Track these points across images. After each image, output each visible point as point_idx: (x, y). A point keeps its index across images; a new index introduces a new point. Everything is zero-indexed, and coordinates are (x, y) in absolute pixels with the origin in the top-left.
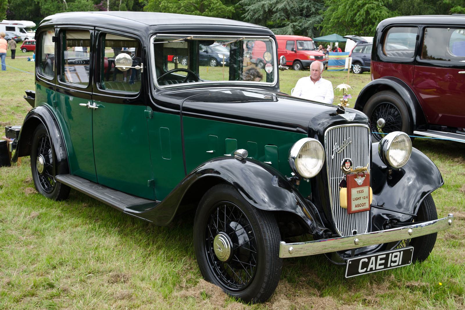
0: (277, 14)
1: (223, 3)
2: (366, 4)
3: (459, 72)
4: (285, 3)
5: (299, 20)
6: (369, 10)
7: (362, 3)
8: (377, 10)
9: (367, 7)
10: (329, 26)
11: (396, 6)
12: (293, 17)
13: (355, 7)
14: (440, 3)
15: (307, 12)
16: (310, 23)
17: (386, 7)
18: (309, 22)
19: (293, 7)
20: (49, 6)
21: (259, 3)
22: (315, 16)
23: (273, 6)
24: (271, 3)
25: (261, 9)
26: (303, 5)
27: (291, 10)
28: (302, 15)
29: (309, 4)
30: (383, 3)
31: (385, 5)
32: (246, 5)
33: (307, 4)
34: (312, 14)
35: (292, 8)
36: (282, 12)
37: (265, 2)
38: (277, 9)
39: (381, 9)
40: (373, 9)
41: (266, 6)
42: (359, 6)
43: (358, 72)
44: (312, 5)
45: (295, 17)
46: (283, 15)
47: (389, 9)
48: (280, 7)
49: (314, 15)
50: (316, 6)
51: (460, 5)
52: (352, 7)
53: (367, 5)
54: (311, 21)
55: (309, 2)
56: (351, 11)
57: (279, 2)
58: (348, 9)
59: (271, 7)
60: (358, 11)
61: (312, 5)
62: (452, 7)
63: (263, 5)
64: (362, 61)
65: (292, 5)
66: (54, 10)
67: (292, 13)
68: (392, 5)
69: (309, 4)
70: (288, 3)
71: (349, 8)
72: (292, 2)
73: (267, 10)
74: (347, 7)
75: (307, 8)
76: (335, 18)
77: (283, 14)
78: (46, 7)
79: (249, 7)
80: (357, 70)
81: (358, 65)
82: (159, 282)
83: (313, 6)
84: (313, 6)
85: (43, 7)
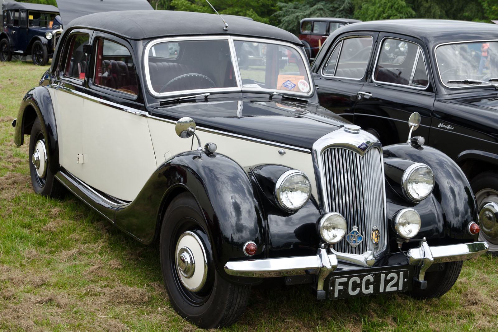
7: (387, 16)
57: (312, 14)
72: (325, 14)
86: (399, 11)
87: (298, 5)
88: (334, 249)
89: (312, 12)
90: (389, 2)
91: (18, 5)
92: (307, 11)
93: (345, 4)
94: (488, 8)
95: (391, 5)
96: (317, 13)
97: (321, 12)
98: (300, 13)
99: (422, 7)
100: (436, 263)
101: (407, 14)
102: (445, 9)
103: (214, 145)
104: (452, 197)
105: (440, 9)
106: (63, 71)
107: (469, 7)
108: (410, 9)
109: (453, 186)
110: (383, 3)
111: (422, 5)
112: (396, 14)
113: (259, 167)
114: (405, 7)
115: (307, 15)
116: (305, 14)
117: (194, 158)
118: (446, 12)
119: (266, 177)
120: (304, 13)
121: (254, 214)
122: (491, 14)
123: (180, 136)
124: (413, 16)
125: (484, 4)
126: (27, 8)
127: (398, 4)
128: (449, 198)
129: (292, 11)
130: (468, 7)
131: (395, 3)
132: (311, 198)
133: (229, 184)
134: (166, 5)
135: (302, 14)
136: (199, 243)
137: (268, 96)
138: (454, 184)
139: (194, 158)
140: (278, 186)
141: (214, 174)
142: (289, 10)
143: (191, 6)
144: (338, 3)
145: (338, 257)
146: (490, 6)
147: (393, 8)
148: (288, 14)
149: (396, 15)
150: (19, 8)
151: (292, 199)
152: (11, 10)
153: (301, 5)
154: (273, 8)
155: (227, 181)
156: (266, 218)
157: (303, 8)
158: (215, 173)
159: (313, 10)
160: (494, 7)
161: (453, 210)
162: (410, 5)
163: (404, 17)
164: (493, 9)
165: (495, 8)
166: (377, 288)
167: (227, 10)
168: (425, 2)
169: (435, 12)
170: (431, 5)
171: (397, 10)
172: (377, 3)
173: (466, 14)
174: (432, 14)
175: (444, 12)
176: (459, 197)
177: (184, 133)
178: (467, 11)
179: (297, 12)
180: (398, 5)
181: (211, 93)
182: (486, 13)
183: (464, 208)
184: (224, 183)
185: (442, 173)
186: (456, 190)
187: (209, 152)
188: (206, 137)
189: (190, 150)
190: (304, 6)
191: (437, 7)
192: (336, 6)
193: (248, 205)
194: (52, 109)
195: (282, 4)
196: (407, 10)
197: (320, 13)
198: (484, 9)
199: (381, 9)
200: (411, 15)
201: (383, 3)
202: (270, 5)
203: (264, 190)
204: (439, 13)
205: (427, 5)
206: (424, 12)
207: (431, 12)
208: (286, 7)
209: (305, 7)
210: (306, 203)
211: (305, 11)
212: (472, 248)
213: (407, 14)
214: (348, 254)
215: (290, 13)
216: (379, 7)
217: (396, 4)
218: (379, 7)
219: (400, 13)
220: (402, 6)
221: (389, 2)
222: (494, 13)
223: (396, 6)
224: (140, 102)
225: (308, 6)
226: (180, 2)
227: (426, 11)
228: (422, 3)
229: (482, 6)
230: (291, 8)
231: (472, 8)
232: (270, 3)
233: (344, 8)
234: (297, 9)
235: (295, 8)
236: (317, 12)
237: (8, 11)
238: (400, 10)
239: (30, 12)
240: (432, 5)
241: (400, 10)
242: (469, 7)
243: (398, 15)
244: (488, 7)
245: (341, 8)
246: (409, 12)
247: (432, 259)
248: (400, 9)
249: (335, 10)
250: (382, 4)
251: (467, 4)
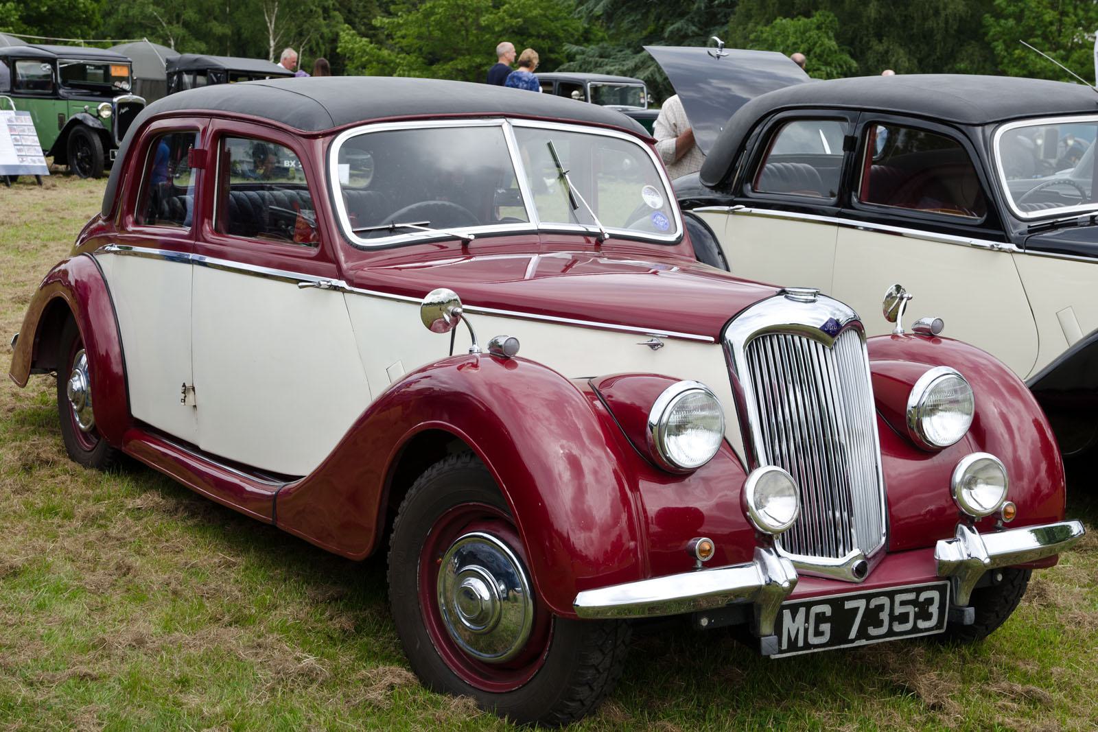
30: (839, 70)
57: (640, 68)
86: (823, 59)
87: (609, 50)
88: (784, 548)
89: (639, 64)
90: (802, 42)
91: (207, 61)
92: (628, 62)
94: (1006, 54)
95: (807, 49)
96: (649, 67)
98: (612, 66)
99: (870, 52)
100: (995, 566)
101: (841, 66)
102: (918, 56)
103: (513, 341)
104: (1006, 436)
106: (751, 182)
107: (966, 51)
108: (846, 57)
109: (1005, 410)
110: (790, 45)
111: (870, 48)
112: (816, 66)
113: (608, 382)
114: (836, 52)
115: (628, 70)
116: (625, 68)
117: (460, 368)
118: (920, 61)
119: (628, 402)
120: (623, 65)
121: (611, 481)
122: (1011, 65)
123: (430, 327)
124: (853, 70)
125: (998, 46)
126: (227, 67)
127: (821, 45)
128: (1000, 437)
129: (596, 63)
130: (964, 52)
131: (815, 44)
132: (725, 443)
133: (553, 420)
134: (320, 51)
135: (617, 67)
136: (876, 463)
137: (593, 240)
138: (1007, 407)
139: (460, 368)
140: (653, 418)
141: (513, 398)
142: (590, 59)
143: (380, 53)
145: (796, 565)
146: (1009, 50)
148: (589, 68)
149: (818, 69)
150: (206, 67)
151: (689, 449)
152: (188, 72)
153: (614, 49)
154: (553, 56)
155: (547, 413)
156: (635, 487)
157: (619, 55)
158: (514, 396)
159: (642, 59)
160: (1017, 52)
161: (1011, 462)
162: (844, 47)
163: (835, 72)
164: (1016, 56)
165: (1019, 54)
166: (839, 634)
167: (459, 61)
168: (877, 42)
169: (897, 61)
170: (888, 47)
171: (819, 57)
172: (779, 45)
173: (962, 66)
175: (915, 61)
176: (1020, 436)
177: (435, 320)
178: (962, 60)
179: (606, 65)
180: (823, 47)
181: (478, 236)
182: (1001, 63)
183: (1032, 458)
184: (539, 419)
185: (981, 385)
186: (1014, 422)
187: (503, 355)
188: (490, 328)
189: (448, 355)
190: (621, 51)
191: (901, 52)
193: (600, 463)
194: (714, 245)
195: (575, 48)
196: (841, 58)
198: (999, 55)
200: (850, 68)
201: (790, 45)
202: (547, 50)
203: (627, 428)
204: (907, 64)
205: (880, 48)
206: (876, 63)
208: (583, 53)
209: (624, 53)
210: (717, 456)
211: (624, 63)
212: (1047, 537)
213: (841, 66)
214: (806, 556)
215: (592, 66)
217: (818, 45)
219: (827, 64)
220: (830, 49)
221: (802, 42)
222: (1019, 63)
223: (818, 50)
224: (988, 221)
225: (628, 51)
226: (356, 46)
227: (878, 61)
228: (871, 43)
229: (992, 50)
230: (593, 56)
231: (972, 54)
232: (547, 46)
234: (608, 57)
235: (601, 56)
237: (180, 73)
238: (826, 59)
239: (231, 74)
240: (891, 47)
241: (826, 59)
242: (966, 51)
243: (823, 68)
244: (1006, 51)
246: (845, 62)
247: (987, 561)
248: (825, 56)
250: (788, 46)
251: (961, 45)
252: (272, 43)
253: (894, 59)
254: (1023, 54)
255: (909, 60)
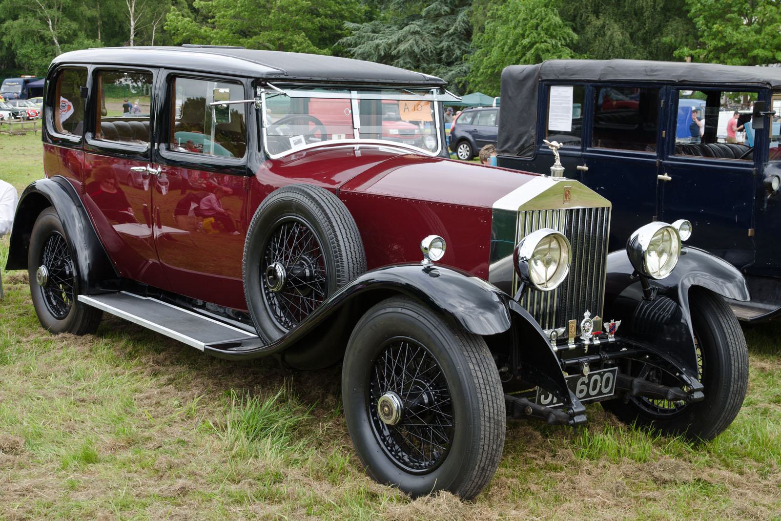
0: (399, 60)
1: (312, 42)
2: (536, 43)
3: (132, 168)
4: (411, 41)
5: (434, 69)
6: (541, 53)
7: (529, 43)
8: (554, 53)
9: (537, 49)
10: (479, 79)
11: (587, 46)
12: (425, 65)
13: (518, 48)
14: (657, 42)
15: (449, 56)
16: (453, 74)
17: (571, 49)
18: (450, 73)
19: (424, 49)
20: (29, 50)
21: (370, 42)
22: (462, 63)
23: (393, 47)
24: (390, 41)
25: (373, 52)
26: (441, 46)
27: (422, 53)
28: (440, 61)
29: (451, 43)
30: (563, 42)
31: (567, 45)
32: (350, 45)
33: (447, 43)
34: (457, 59)
35: (423, 50)
36: (408, 56)
37: (381, 42)
38: (399, 52)
39: (560, 51)
40: (548, 51)
41: (381, 47)
42: (524, 47)
43: (466, 157)
44: (456, 46)
45: (428, 64)
46: (409, 62)
47: (574, 51)
48: (403, 49)
49: (459, 62)
50: (463, 48)
51: (687, 46)
52: (515, 49)
53: (538, 45)
54: (453, 72)
55: (452, 40)
56: (512, 55)
57: (402, 41)
58: (507, 52)
59: (390, 49)
60: (524, 54)
61: (456, 46)
62: (676, 49)
63: (378, 46)
64: (470, 137)
65: (423, 46)
66: (37, 56)
67: (423, 59)
68: (581, 45)
69: (451, 43)
70: (417, 42)
71: (510, 49)
72: (424, 41)
73: (383, 54)
74: (506, 49)
75: (448, 51)
76: (486, 67)
77: (408, 60)
78: (23, 51)
79: (355, 49)
80: (464, 154)
81: (465, 146)
82: (697, 478)
83: (458, 47)
84: (458, 47)
85: (18, 52)
89: (402, 38)
93: (457, 23)
97: (417, 37)
105: (621, 30)
144: (446, 21)
147: (539, 29)
164: (714, 30)
165: (718, 28)
169: (612, 34)
174: (607, 38)
175: (628, 35)
191: (616, 26)
192: (442, 27)
197: (415, 40)
199: (519, 30)
207: (605, 35)
216: (515, 28)
218: (515, 28)
233: (456, 29)
235: (374, 32)
236: (410, 37)
243: (549, 40)
245: (451, 31)
249: (441, 34)
252: (132, 23)
253: (609, 33)
254: (721, 28)
255: (622, 33)
